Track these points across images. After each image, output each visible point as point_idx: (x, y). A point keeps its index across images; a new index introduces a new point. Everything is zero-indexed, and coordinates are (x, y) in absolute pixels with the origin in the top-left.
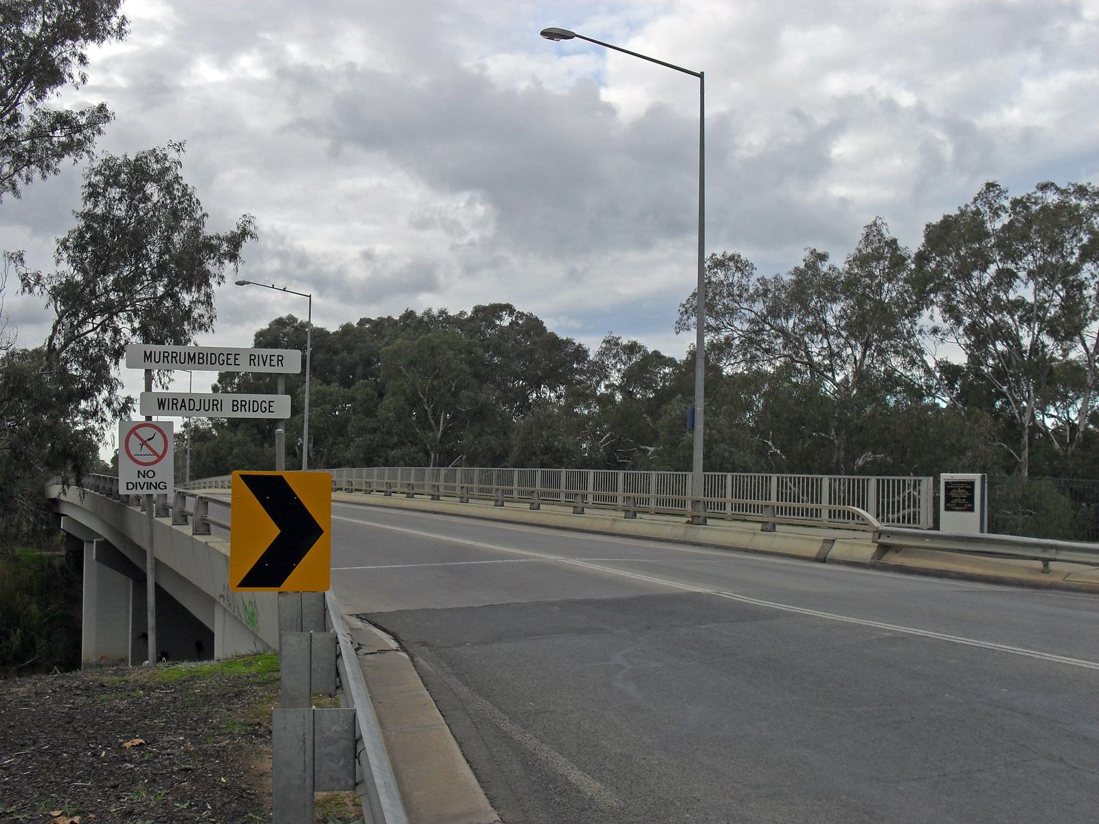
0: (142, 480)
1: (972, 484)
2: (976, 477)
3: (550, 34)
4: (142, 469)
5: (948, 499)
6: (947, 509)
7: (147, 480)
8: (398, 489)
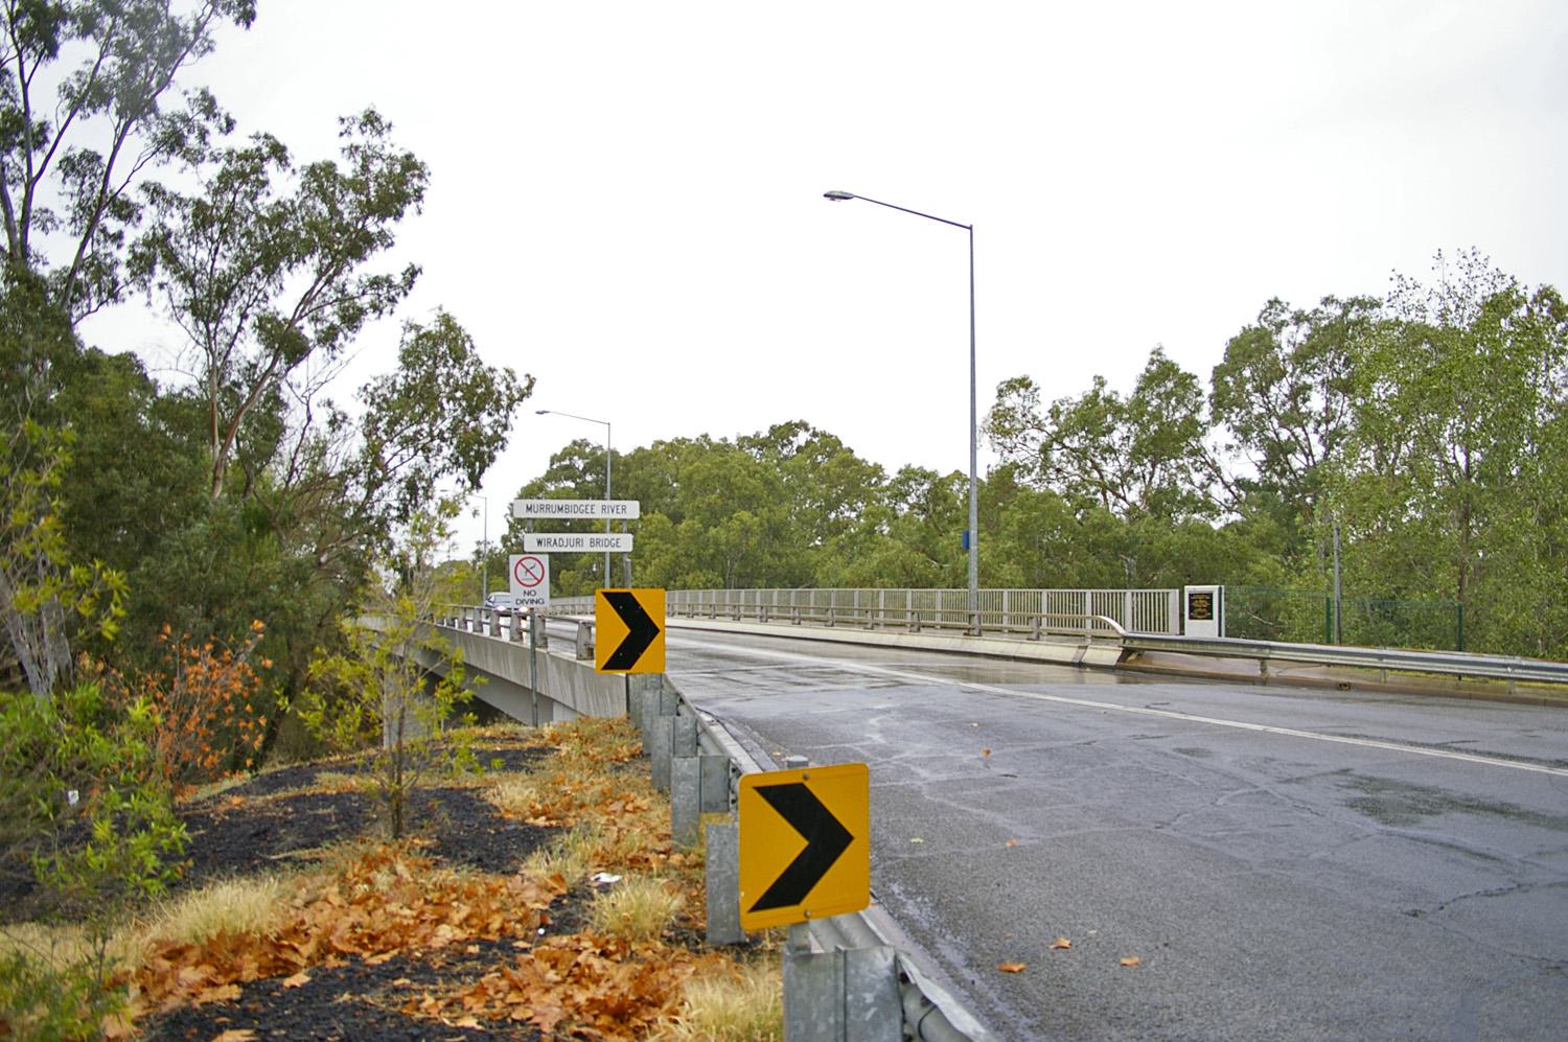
0: (527, 598)
1: (1211, 595)
2: (1214, 589)
3: (831, 196)
4: (527, 589)
5: (1191, 609)
6: (1191, 618)
7: (530, 597)
8: (700, 610)
